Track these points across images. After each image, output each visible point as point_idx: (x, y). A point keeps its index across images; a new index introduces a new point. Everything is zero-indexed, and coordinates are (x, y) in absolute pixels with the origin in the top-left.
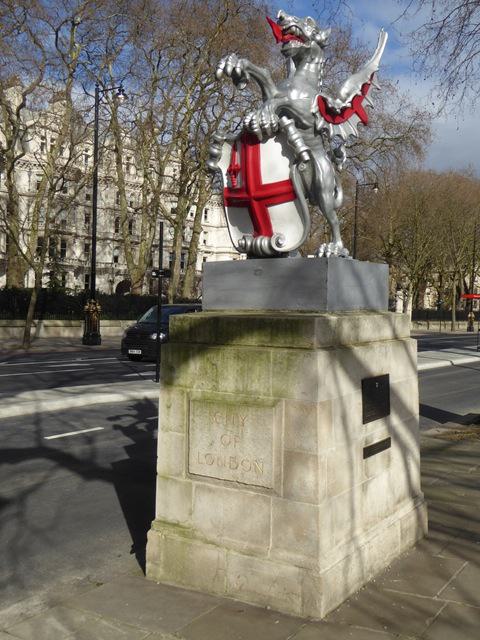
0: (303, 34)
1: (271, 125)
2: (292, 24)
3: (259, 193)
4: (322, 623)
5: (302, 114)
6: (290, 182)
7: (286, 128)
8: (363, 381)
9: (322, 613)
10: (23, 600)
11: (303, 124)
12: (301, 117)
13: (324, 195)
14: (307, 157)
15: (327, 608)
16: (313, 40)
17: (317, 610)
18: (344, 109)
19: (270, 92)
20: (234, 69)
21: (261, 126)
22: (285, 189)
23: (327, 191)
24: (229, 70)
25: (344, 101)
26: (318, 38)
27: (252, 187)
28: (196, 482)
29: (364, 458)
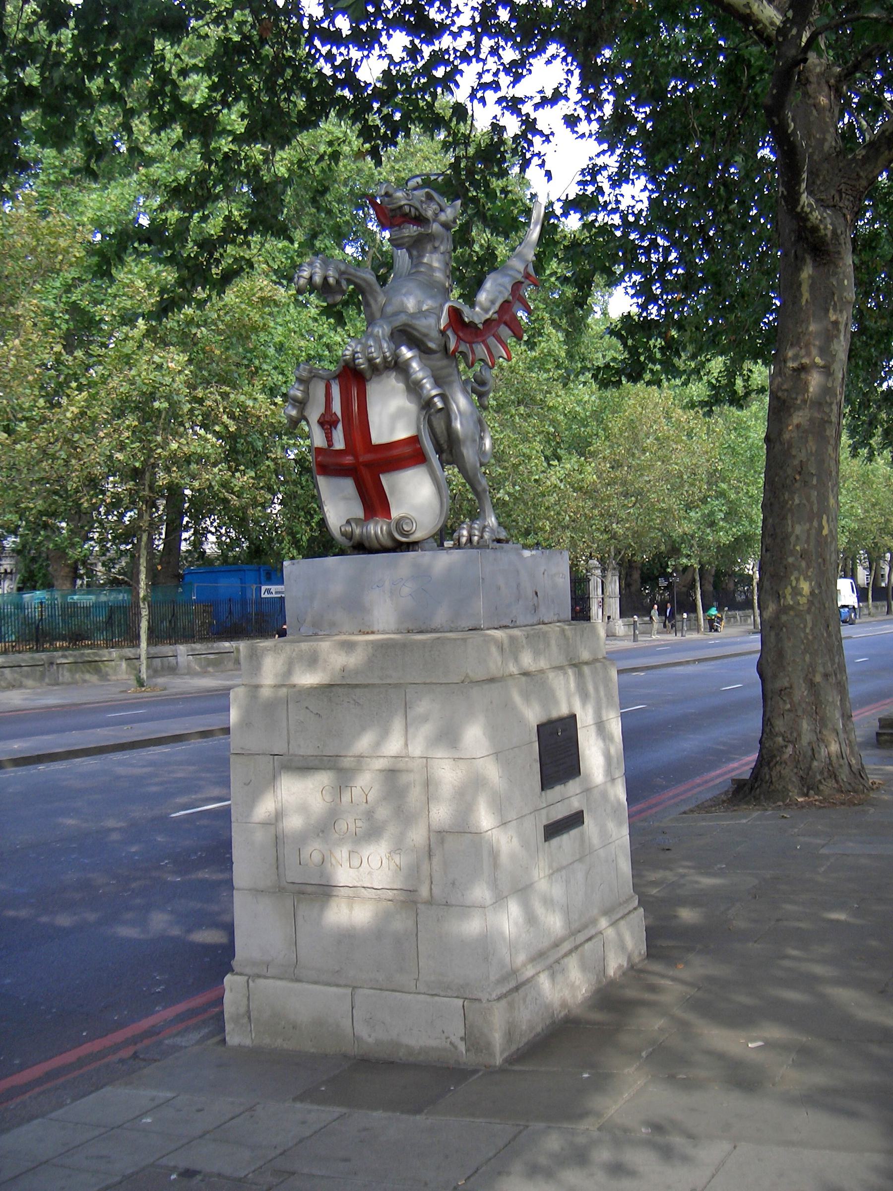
0: (420, 214)
1: (385, 358)
2: (403, 203)
3: (368, 457)
4: (502, 1070)
5: (426, 335)
6: (415, 440)
7: (407, 363)
8: (579, 772)
9: (498, 1061)
10: (837, 484)
11: (430, 349)
12: (425, 339)
13: (465, 452)
14: (440, 405)
15: (502, 1053)
16: (434, 221)
17: (492, 1055)
18: (487, 322)
19: (376, 301)
20: (325, 279)
21: (370, 361)
22: (407, 450)
23: (468, 443)
24: (318, 279)
25: (486, 311)
26: (443, 217)
27: (359, 446)
28: (28, 1095)
29: (543, 789)
